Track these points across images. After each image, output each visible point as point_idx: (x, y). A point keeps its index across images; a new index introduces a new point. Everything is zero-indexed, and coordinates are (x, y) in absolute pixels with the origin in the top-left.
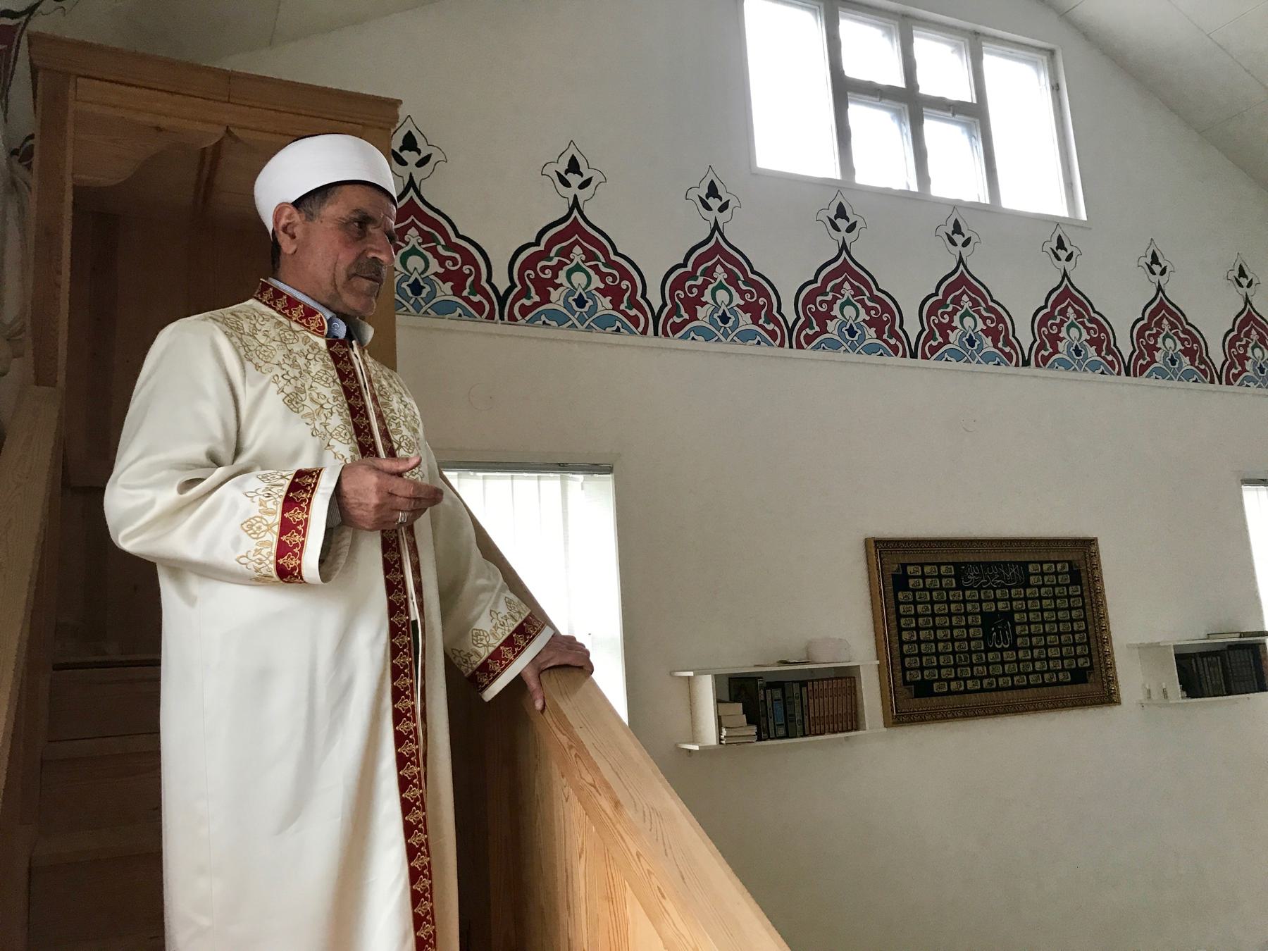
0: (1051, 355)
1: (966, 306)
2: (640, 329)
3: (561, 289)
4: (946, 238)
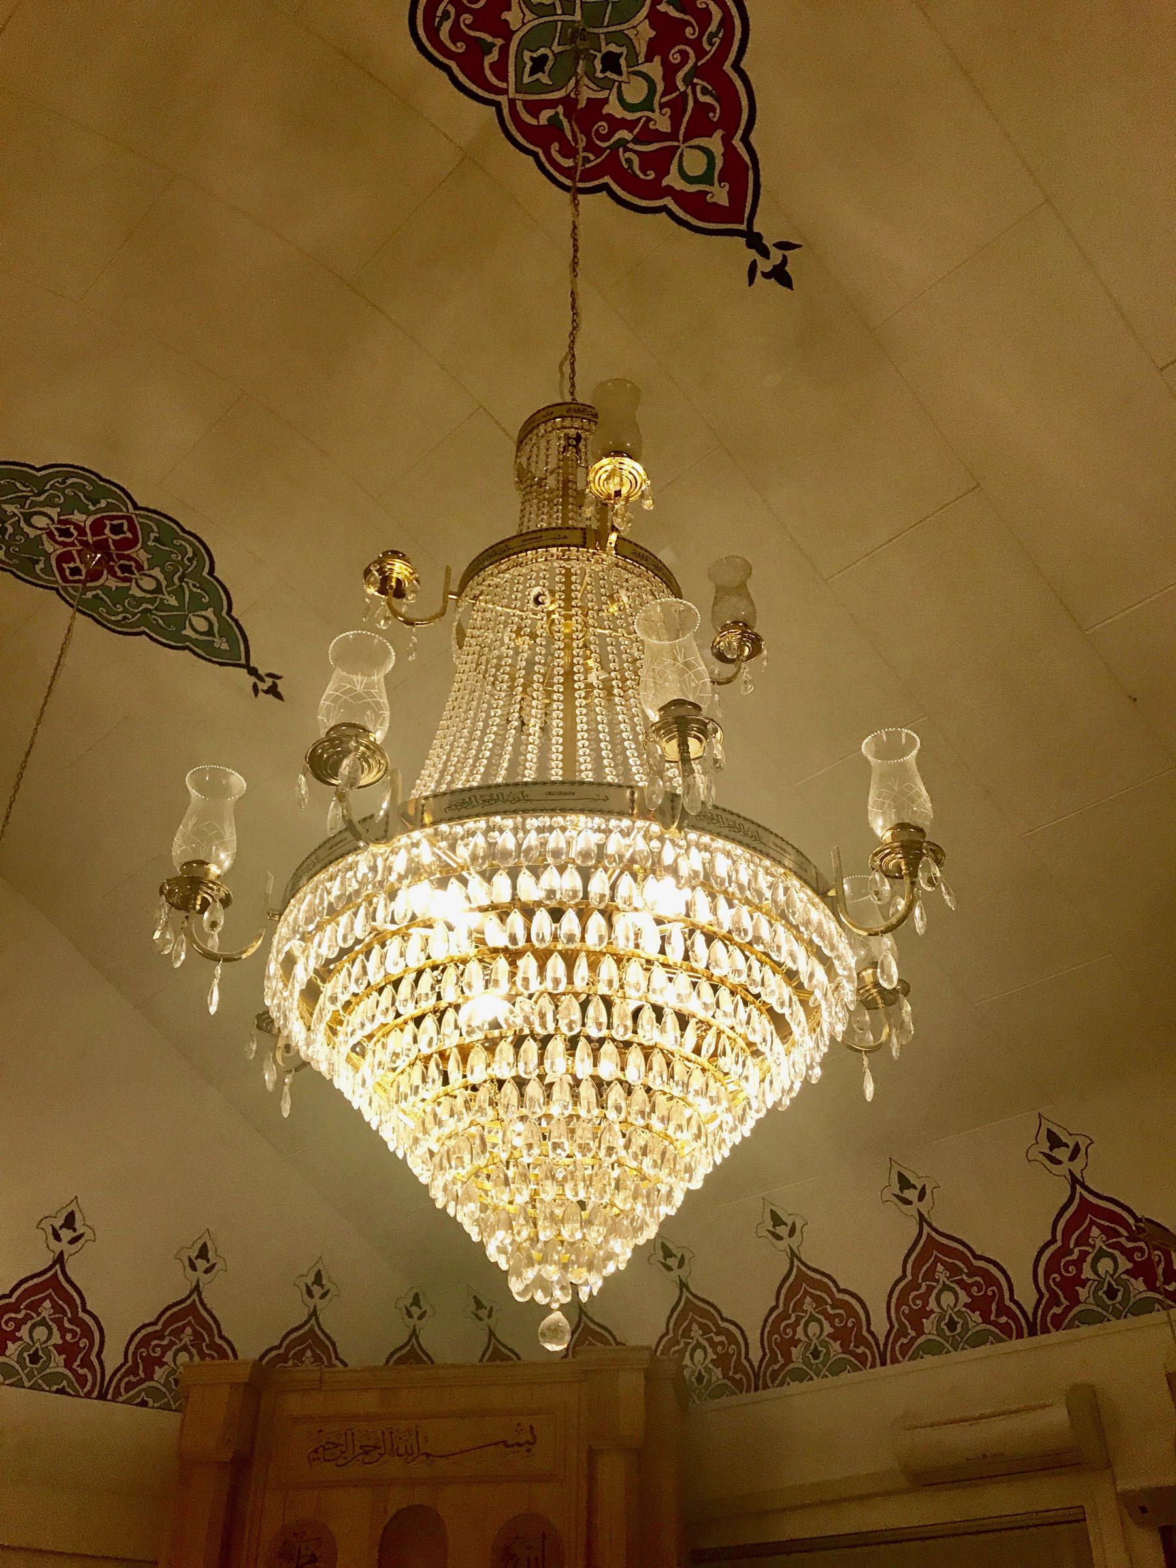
0: (1068, 1310)
1: (1099, 1243)
2: (86, 1390)
3: (18, 1343)
4: (895, 1199)
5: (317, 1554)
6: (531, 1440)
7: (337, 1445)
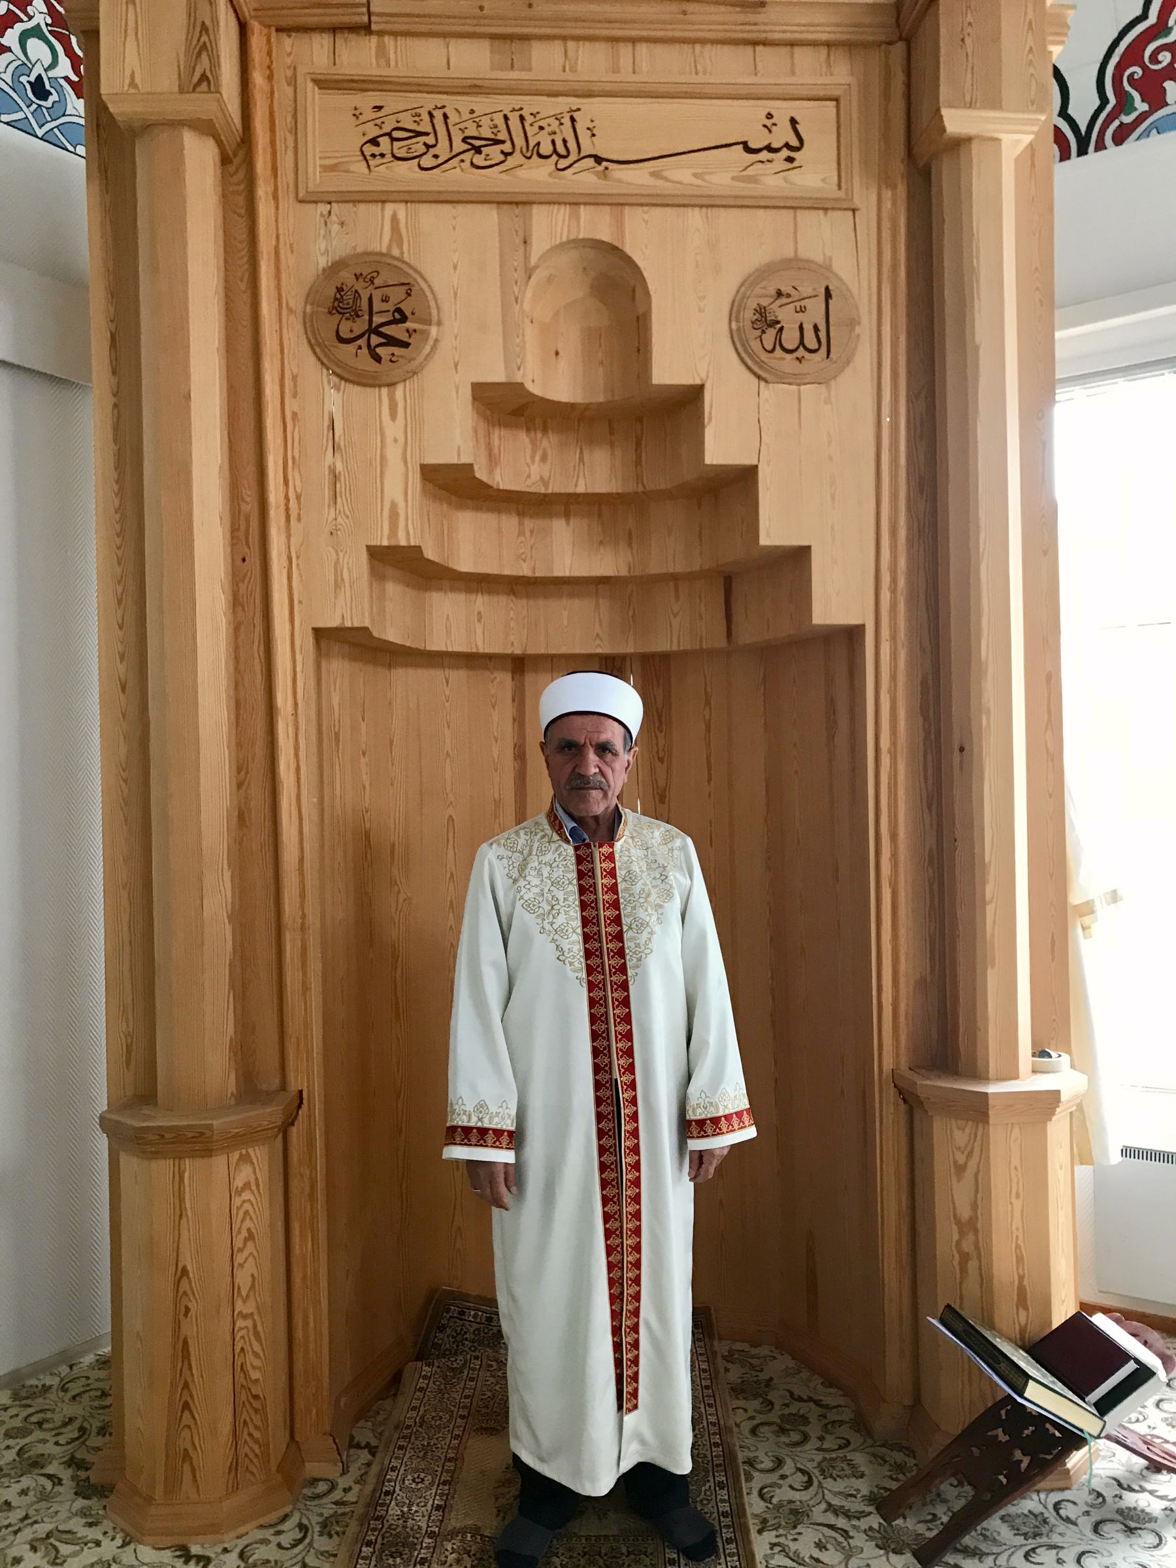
5: (406, 308)
6: (794, 142)
7: (419, 134)
